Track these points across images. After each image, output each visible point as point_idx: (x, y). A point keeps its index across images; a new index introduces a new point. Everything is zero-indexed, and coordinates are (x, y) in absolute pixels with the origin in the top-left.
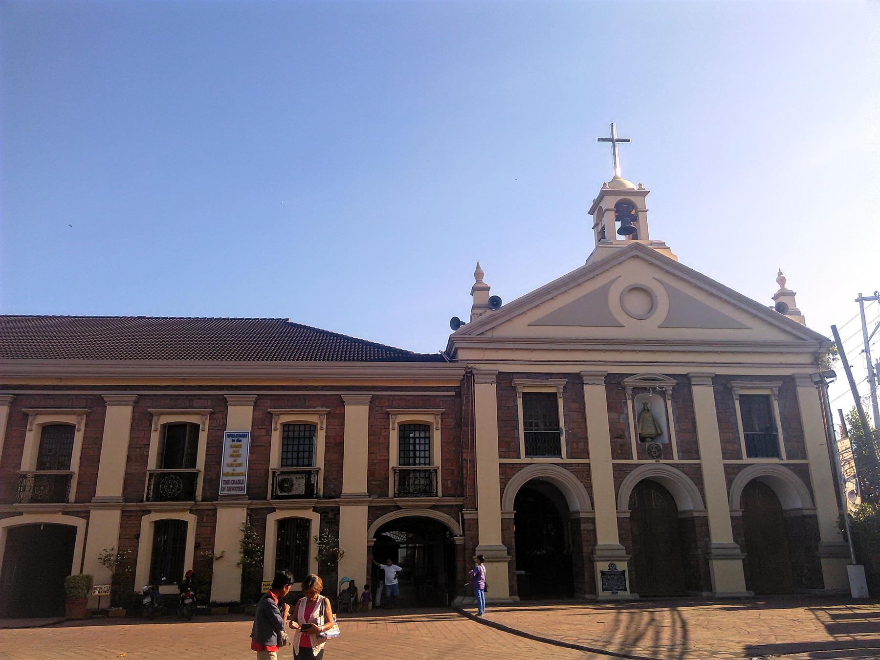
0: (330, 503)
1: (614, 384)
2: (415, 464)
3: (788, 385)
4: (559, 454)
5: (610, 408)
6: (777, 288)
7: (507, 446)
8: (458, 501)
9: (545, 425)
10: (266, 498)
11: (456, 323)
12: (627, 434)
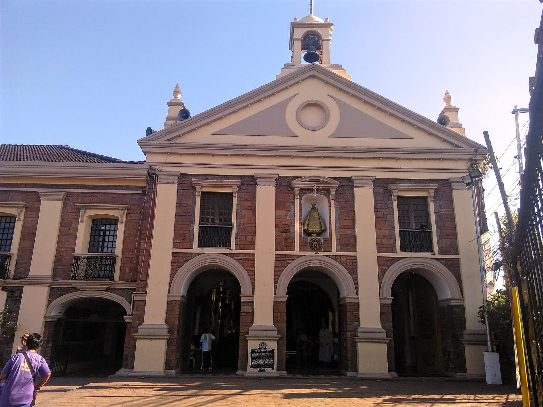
0: (16, 283)
1: (284, 185)
2: (102, 252)
3: (444, 189)
4: (229, 245)
5: (279, 206)
6: (445, 105)
7: (181, 236)
8: (133, 285)
9: (221, 221)
10: (111, 278)
11: (149, 131)
12: (291, 228)
